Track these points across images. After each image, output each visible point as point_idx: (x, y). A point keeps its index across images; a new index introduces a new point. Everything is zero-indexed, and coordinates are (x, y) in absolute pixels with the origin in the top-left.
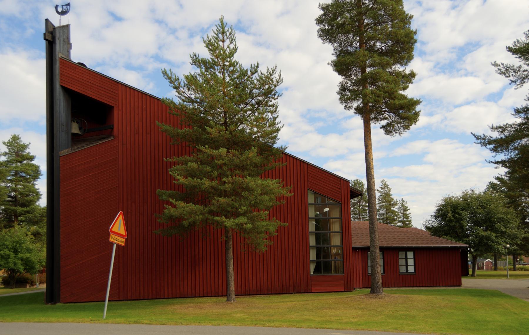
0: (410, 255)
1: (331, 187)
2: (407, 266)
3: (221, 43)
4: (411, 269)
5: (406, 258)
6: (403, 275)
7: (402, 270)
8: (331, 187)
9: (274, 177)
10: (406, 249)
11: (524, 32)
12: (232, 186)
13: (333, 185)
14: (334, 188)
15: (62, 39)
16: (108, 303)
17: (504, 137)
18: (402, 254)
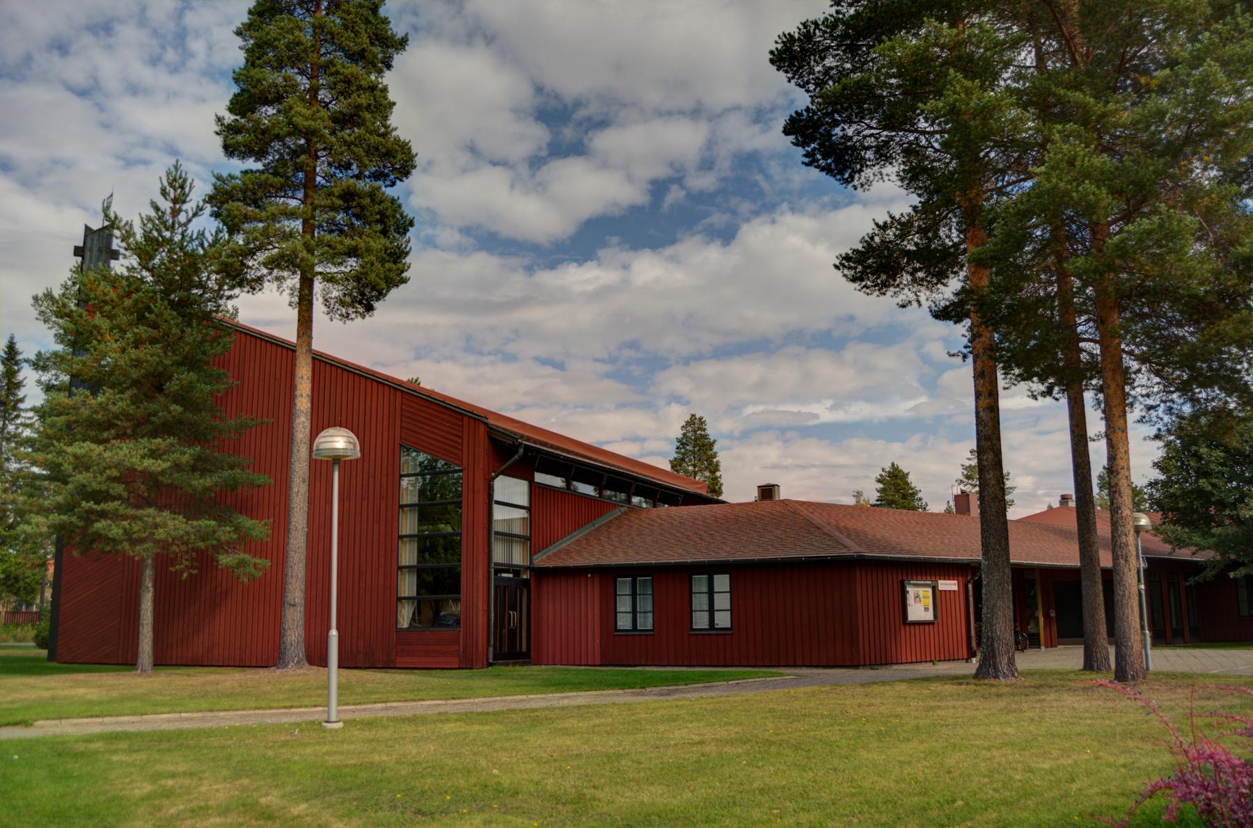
0: (722, 582)
1: (444, 434)
2: (711, 610)
3: (167, 234)
4: (646, 622)
5: (711, 593)
6: (701, 634)
7: (701, 621)
8: (444, 434)
9: (231, 452)
10: (712, 569)
11: (34, 294)
12: (972, 315)
13: (448, 429)
14: (450, 437)
15: (95, 249)
16: (339, 675)
17: (170, 419)
18: (624, 587)
